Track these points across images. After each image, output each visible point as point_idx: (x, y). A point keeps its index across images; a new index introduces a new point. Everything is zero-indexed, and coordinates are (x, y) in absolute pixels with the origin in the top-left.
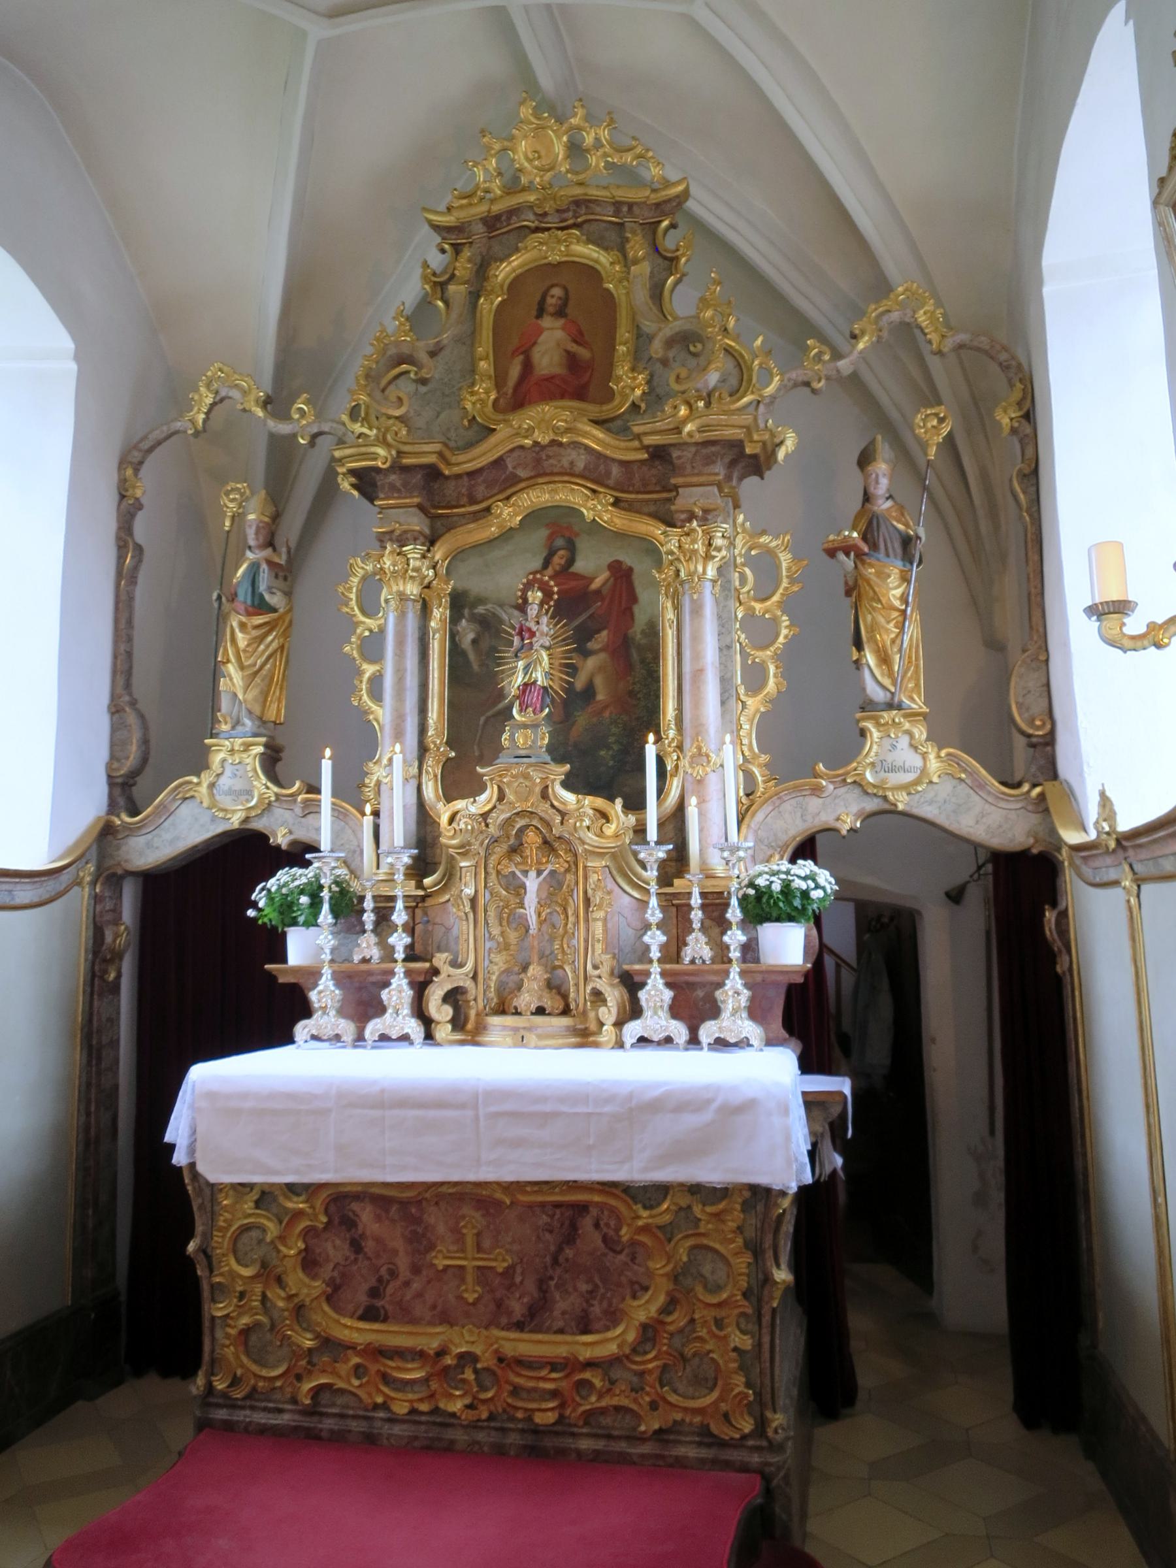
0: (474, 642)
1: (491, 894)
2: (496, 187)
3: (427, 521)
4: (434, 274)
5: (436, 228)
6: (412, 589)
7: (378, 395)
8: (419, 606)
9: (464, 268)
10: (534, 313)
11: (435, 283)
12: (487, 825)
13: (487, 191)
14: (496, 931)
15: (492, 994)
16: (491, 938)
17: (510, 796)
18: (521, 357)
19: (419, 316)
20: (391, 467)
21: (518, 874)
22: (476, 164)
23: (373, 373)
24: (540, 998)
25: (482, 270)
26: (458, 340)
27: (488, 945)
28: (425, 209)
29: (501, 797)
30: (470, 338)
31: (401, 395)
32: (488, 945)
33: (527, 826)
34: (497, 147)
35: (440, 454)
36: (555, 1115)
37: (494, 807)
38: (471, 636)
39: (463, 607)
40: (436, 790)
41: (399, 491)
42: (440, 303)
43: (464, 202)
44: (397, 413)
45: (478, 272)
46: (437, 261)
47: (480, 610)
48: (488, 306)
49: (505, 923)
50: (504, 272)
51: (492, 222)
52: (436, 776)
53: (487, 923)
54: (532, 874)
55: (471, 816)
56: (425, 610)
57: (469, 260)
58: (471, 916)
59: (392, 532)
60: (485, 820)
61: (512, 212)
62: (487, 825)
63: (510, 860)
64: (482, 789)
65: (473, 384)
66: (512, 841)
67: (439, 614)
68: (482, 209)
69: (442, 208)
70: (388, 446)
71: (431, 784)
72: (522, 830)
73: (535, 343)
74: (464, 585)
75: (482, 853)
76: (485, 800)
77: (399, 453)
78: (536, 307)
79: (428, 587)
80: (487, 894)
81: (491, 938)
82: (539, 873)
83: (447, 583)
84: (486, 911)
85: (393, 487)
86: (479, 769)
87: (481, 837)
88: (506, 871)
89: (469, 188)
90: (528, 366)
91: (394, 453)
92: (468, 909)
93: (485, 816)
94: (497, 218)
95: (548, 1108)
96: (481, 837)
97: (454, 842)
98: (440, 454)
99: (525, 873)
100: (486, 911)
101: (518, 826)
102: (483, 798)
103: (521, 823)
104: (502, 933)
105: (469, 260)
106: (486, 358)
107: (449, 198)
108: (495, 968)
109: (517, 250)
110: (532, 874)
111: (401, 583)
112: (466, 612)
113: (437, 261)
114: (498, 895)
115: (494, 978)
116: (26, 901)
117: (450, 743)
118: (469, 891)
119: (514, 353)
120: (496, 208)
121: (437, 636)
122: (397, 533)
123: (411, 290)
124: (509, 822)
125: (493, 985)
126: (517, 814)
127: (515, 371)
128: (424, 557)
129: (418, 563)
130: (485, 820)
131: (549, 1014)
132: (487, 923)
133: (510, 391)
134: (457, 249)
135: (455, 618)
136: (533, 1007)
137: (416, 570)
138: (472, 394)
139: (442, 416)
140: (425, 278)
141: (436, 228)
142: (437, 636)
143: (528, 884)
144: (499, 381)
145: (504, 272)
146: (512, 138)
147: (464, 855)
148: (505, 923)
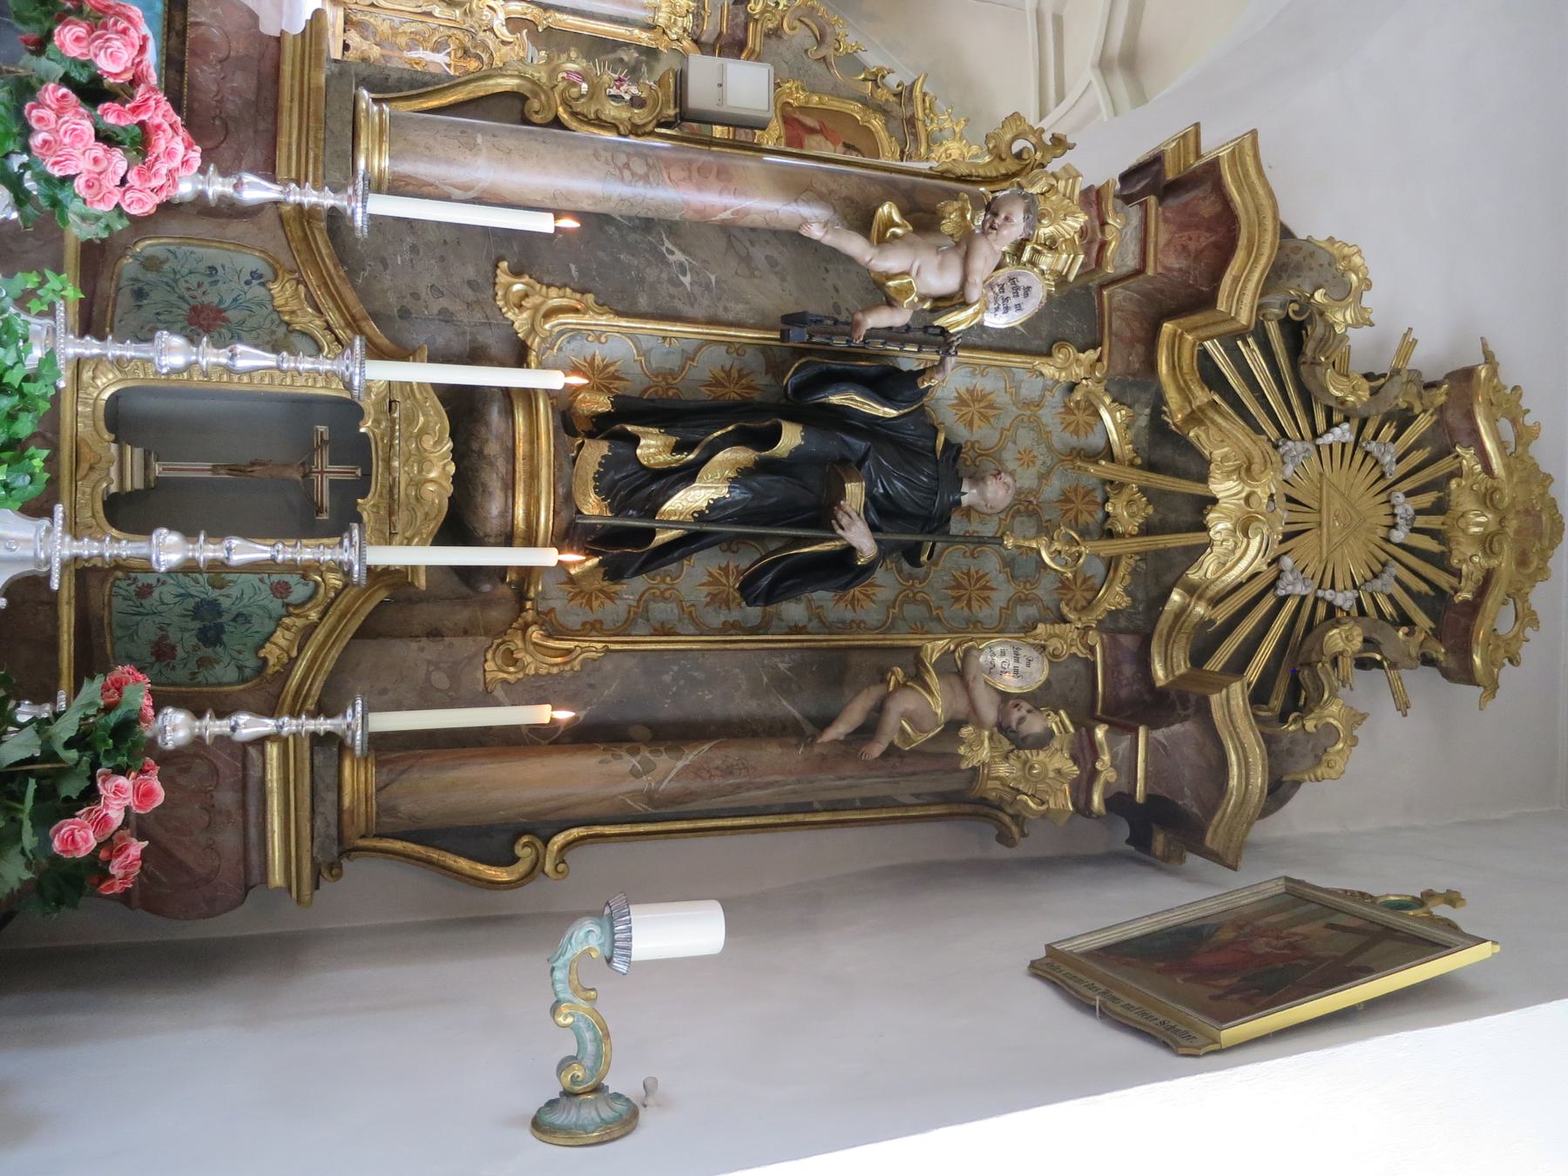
0: (622, 60)
1: (434, 29)
2: (933, 127)
3: (711, 41)
4: (883, 77)
5: (913, 84)
6: (662, 19)
7: (799, 13)
8: (650, 22)
9: (882, 95)
10: (847, 142)
11: (877, 75)
12: (485, 31)
13: (932, 120)
14: (407, 28)
15: (359, 17)
16: (402, 23)
17: (505, 49)
18: (818, 128)
19: (852, 62)
20: (748, 13)
21: (448, 50)
22: (949, 115)
23: (814, 12)
24: (355, 48)
25: (882, 110)
26: (835, 86)
27: (397, 20)
28: (926, 76)
29: (503, 42)
30: (836, 93)
31: (797, 30)
32: (397, 20)
33: (482, 62)
34: (957, 129)
35: (753, 51)
36: (280, 12)
37: (497, 38)
38: (626, 58)
39: (647, 56)
40: (515, 13)
41: (733, 20)
42: (862, 76)
43: (928, 104)
44: (785, 25)
45: (880, 106)
46: (892, 81)
47: (644, 69)
48: (855, 109)
49: (412, 36)
50: (877, 123)
51: (911, 121)
52: (525, 14)
53: (413, 21)
54: (447, 60)
55: (491, 20)
56: (650, 27)
57: (887, 100)
58: (419, 10)
59: (704, 9)
60: (489, 30)
61: (915, 136)
62: (485, 31)
63: (459, 48)
64: (512, 32)
65: (804, 90)
66: (473, 51)
67: (644, 38)
68: (920, 115)
69: (926, 89)
70: (763, 12)
71: (519, 8)
72: (479, 58)
73: (827, 139)
74: (663, 58)
75: (464, 27)
76: (503, 33)
77: (756, 21)
78: (851, 143)
79: (664, 32)
80: (435, 26)
81: (402, 23)
82: (449, 65)
83: (666, 47)
84: (422, 22)
85: (736, 15)
86: (525, 31)
87: (476, 26)
88: (450, 41)
89: (936, 109)
90: (812, 131)
91: (757, 17)
92: (425, 9)
93: (491, 30)
94: (914, 126)
95: (285, 8)
96: (476, 26)
97: (474, 6)
98: (753, 51)
99: (449, 54)
100: (422, 22)
101: (483, 55)
102: (505, 30)
103: (485, 57)
104: (405, 33)
105: (887, 100)
106: (820, 102)
107: (932, 94)
108: (379, 23)
109: (891, 137)
110: (447, 60)
111: (668, 10)
112: (644, 58)
113: (892, 81)
114: (432, 34)
115: (372, 20)
116: (316, 762)
117: (548, 29)
118: (437, 12)
119: (822, 123)
120: (919, 124)
121: (628, 33)
122: (703, 12)
123: (873, 60)
124: (486, 48)
125: (366, 18)
126: (492, 54)
127: (809, 121)
128: (685, 30)
129: (680, 24)
130: (489, 30)
131: (343, 54)
132: (413, 21)
133: (796, 116)
134: (898, 95)
135: (639, 48)
136: (349, 42)
137: (675, 22)
138: (797, 88)
139: (785, 65)
140: (880, 69)
141: (913, 84)
142: (628, 33)
143: (441, 55)
144: (803, 109)
145: (877, 123)
146: (961, 139)
147: (465, 13)
148: (412, 36)
